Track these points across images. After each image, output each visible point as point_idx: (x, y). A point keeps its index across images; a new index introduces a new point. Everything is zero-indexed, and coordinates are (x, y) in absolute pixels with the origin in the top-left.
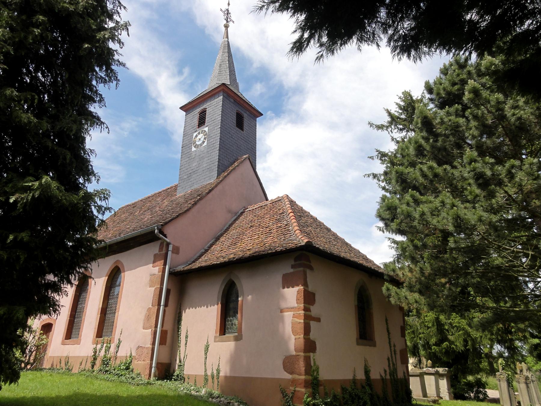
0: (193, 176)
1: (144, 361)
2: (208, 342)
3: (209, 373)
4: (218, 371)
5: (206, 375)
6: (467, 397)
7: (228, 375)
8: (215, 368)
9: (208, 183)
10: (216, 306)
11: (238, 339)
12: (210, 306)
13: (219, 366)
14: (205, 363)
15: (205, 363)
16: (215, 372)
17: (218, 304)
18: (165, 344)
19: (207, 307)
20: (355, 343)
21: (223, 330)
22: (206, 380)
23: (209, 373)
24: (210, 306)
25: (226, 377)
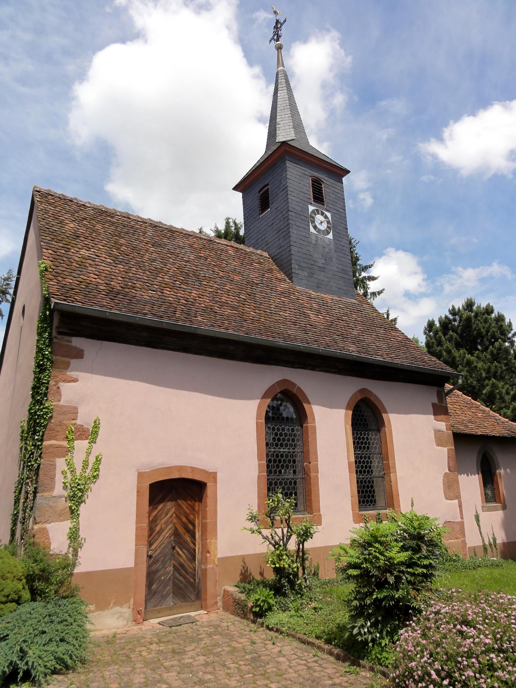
0: (280, 195)
1: (457, 538)
2: (476, 512)
3: (487, 543)
4: (495, 540)
5: (484, 545)
6: (186, 542)
7: (505, 541)
8: (491, 536)
9: (503, 419)
10: (477, 475)
11: (504, 508)
12: (471, 475)
13: (493, 534)
14: (481, 533)
15: (481, 533)
16: (492, 540)
17: (478, 474)
18: (359, 511)
19: (468, 475)
20: (44, 187)
21: (487, 499)
22: (485, 549)
23: (487, 543)
24: (471, 475)
25: (504, 544)
